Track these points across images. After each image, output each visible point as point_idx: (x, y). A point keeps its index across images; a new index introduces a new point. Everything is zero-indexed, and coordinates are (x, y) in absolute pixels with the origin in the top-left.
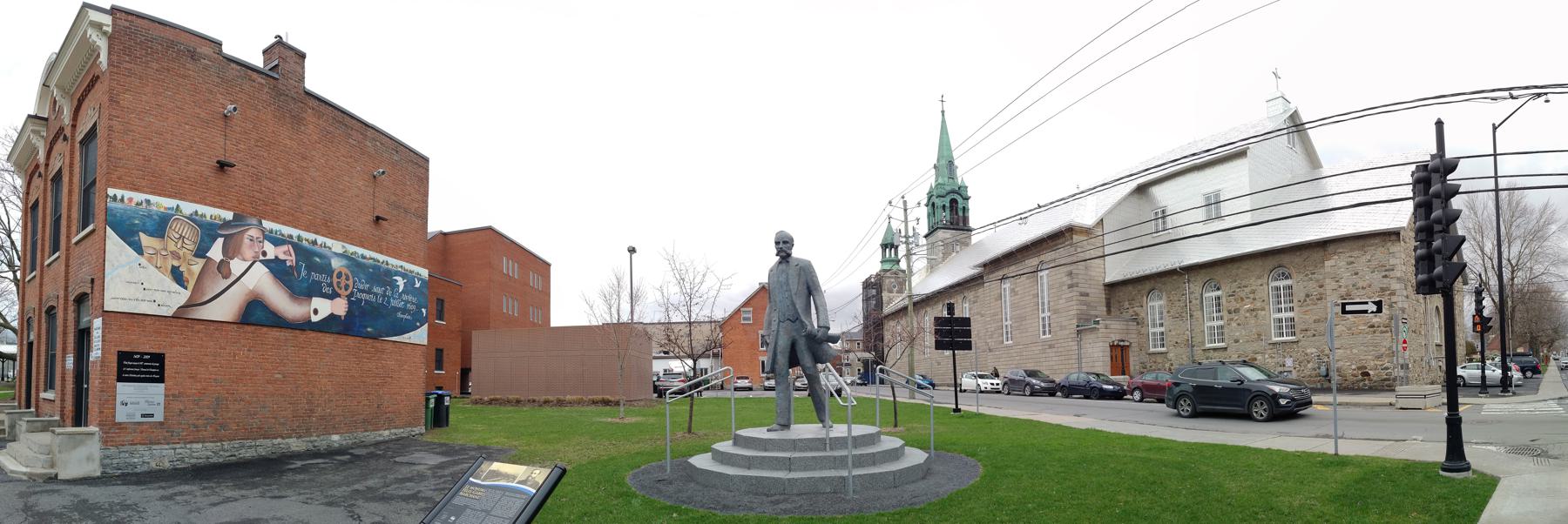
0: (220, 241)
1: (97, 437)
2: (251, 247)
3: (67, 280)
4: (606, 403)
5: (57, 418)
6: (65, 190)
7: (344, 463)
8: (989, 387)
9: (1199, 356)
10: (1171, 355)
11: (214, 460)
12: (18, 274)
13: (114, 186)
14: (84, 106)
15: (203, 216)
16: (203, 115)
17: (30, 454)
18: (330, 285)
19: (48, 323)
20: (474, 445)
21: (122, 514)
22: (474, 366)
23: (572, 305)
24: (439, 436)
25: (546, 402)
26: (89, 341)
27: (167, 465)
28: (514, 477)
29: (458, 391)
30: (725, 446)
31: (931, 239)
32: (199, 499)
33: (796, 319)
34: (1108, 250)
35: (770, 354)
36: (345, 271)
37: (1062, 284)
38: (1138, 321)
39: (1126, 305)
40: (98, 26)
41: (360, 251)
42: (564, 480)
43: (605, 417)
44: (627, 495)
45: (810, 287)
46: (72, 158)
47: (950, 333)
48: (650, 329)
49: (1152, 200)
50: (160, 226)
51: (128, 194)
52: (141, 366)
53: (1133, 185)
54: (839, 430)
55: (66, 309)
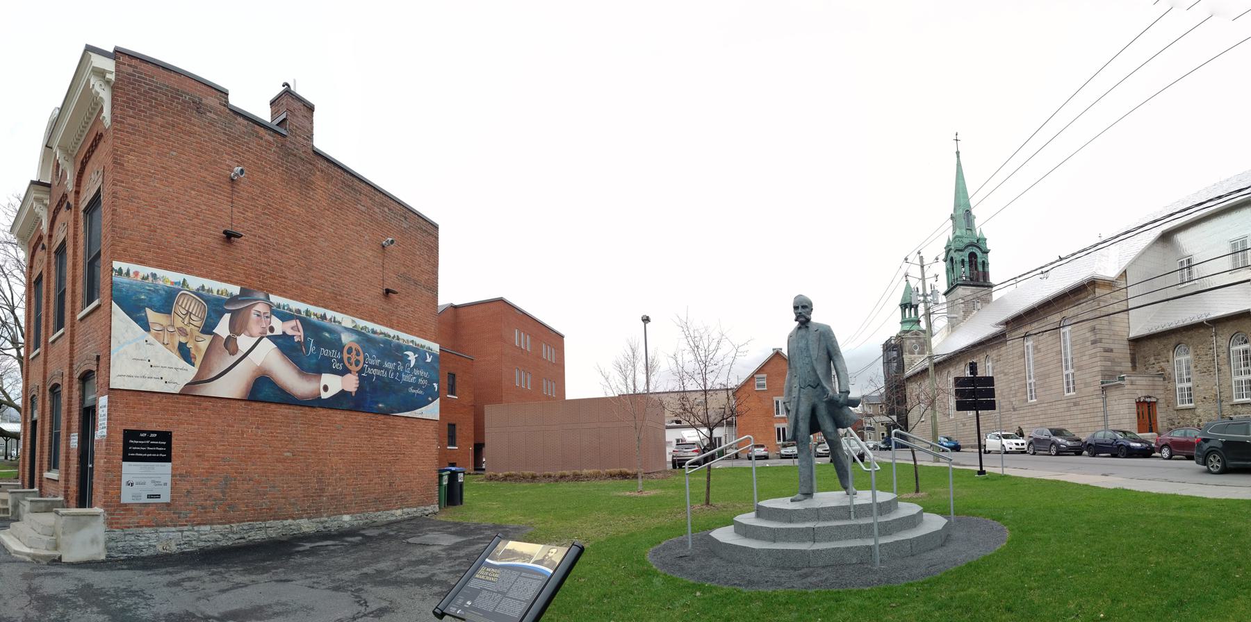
0: (227, 316)
1: (101, 519)
2: (258, 322)
3: (72, 357)
4: (624, 476)
5: (61, 498)
6: (69, 263)
7: (355, 545)
8: (1014, 447)
9: (1228, 411)
10: (1199, 411)
11: (223, 543)
12: (22, 351)
13: (119, 259)
14: (90, 164)
15: (210, 291)
16: (209, 178)
17: (34, 535)
18: (341, 361)
19: (52, 400)
20: (490, 523)
21: (128, 601)
22: (488, 440)
23: (586, 378)
24: (453, 515)
25: (562, 477)
26: (94, 420)
27: (174, 548)
28: (530, 557)
29: (471, 468)
30: (748, 518)
31: (952, 296)
32: (207, 585)
33: (817, 385)
34: (1132, 304)
35: (792, 421)
36: (355, 346)
37: (1085, 340)
38: (1164, 376)
39: (1152, 360)
40: (101, 73)
41: (371, 325)
42: (582, 559)
43: (624, 491)
44: (647, 574)
45: (831, 353)
46: (76, 228)
47: (973, 393)
48: (665, 399)
49: (1176, 248)
50: (167, 301)
51: (133, 267)
52: (147, 445)
53: (1157, 232)
54: (864, 497)
55: (70, 387)
